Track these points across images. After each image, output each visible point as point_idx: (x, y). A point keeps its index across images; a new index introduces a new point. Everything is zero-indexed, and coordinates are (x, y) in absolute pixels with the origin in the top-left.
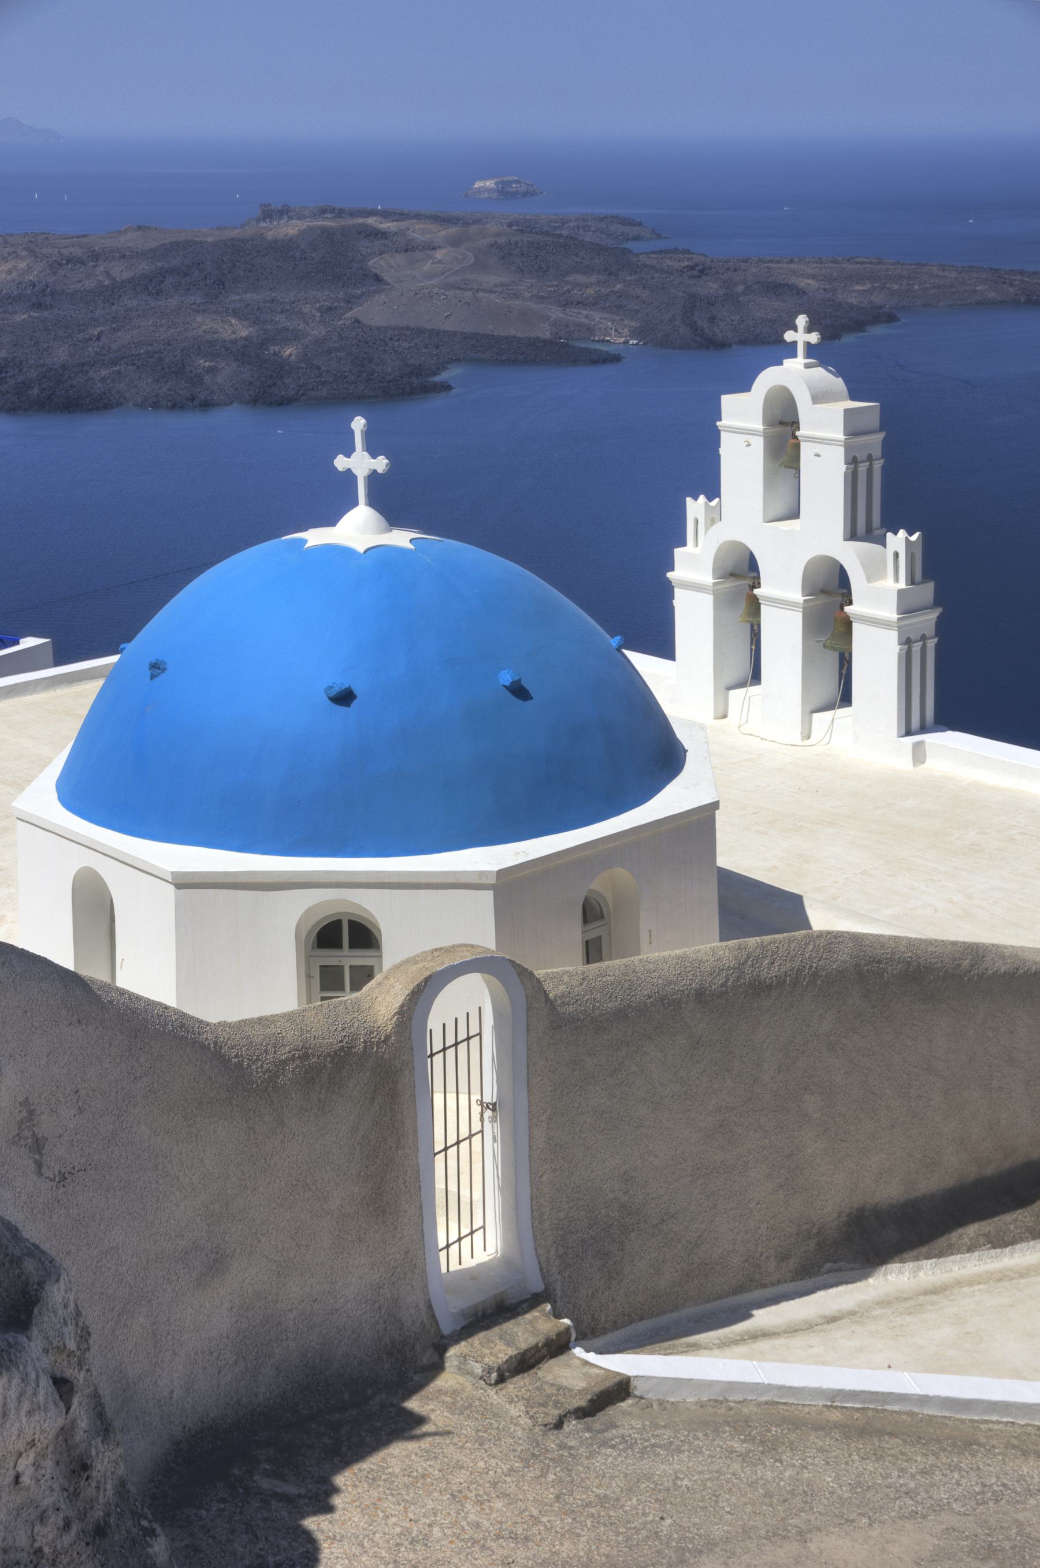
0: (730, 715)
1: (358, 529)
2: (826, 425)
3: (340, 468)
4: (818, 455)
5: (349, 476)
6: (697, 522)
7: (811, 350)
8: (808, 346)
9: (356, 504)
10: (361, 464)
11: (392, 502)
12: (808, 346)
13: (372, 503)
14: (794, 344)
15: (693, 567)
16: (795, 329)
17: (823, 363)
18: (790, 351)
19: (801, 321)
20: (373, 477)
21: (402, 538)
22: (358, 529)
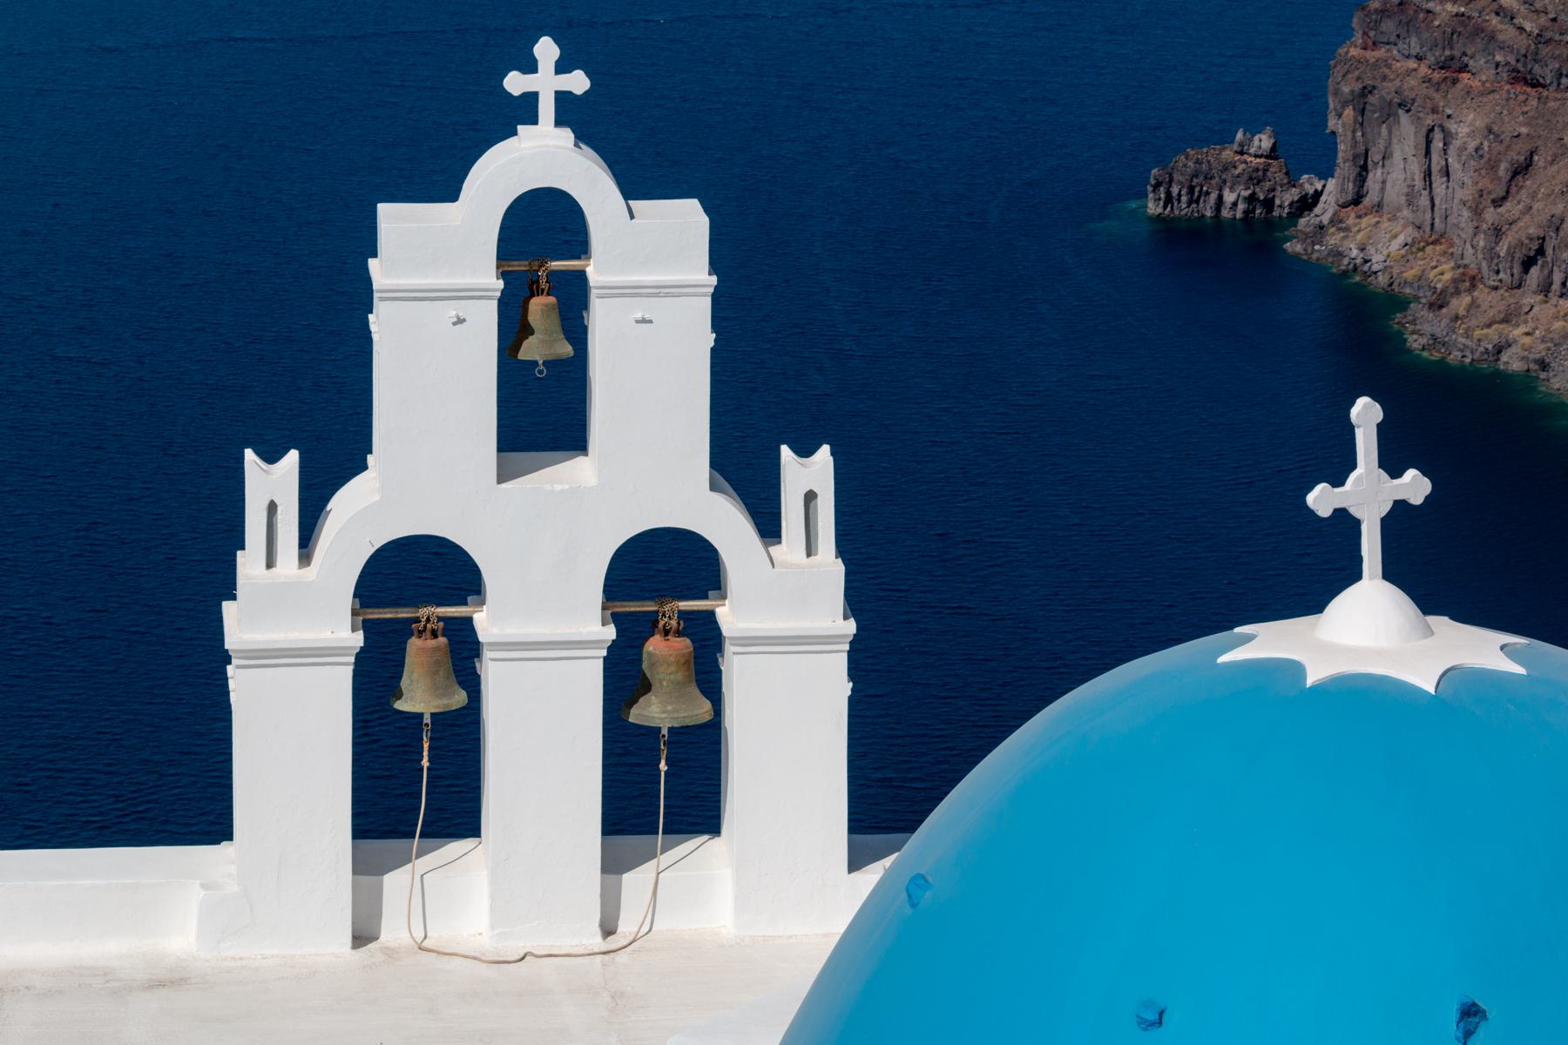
0: (1454, 1016)
1: (1368, 631)
2: (654, 270)
3: (1324, 512)
4: (460, 321)
5: (1345, 523)
6: (272, 508)
7: (569, 110)
8: (562, 98)
9: (1357, 576)
10: (1368, 492)
11: (1435, 568)
12: (562, 98)
13: (1390, 574)
14: (531, 99)
15: (287, 623)
16: (562, 67)
17: (583, 137)
18: (526, 109)
19: (546, 50)
20: (1399, 518)
21: (1485, 650)
22: (1368, 631)
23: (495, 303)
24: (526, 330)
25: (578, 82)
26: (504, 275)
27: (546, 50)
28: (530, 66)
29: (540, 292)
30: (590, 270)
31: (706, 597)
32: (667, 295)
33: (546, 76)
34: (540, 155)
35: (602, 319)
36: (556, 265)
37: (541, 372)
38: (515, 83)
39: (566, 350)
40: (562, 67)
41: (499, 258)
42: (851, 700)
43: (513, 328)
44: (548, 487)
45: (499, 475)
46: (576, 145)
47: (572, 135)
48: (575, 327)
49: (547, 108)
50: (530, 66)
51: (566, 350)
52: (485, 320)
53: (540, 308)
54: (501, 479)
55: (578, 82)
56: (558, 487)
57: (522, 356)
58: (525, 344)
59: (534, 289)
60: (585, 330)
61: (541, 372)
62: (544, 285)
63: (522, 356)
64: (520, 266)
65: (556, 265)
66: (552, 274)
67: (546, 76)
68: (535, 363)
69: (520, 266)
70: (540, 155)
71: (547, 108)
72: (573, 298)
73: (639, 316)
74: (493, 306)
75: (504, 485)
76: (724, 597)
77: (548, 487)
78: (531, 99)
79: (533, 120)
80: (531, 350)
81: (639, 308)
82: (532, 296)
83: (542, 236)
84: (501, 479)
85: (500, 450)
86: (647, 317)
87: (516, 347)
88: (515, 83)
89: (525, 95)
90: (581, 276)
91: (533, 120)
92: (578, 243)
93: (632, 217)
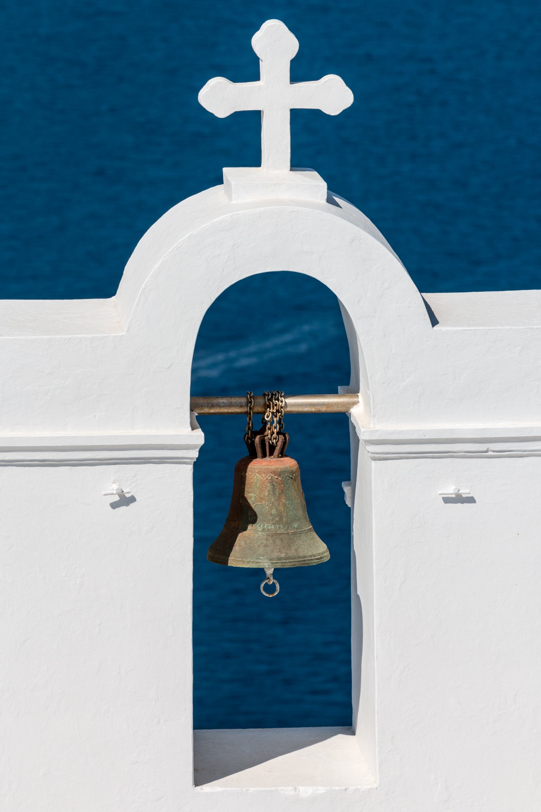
4: (125, 500)
7: (315, 142)
8: (304, 122)
12: (304, 122)
14: (249, 122)
16: (303, 70)
18: (240, 140)
19: (274, 42)
23: (188, 470)
24: (242, 515)
25: (332, 95)
26: (202, 421)
27: (274, 42)
28: (246, 69)
29: (268, 450)
30: (359, 414)
31: (334, 392)
32: (501, 455)
33: (275, 84)
34: (267, 217)
35: (384, 501)
36: (295, 403)
37: (270, 589)
38: (219, 97)
39: (317, 550)
40: (303, 70)
41: (194, 394)
42: (318, 112)
43: (221, 512)
44: (288, 791)
45: (196, 770)
46: (330, 201)
47: (324, 185)
48: (328, 505)
49: (276, 138)
50: (246, 69)
51: (317, 550)
52: (171, 501)
53: (265, 477)
54: (203, 773)
55: (332, 95)
56: (306, 791)
57: (239, 558)
58: (242, 539)
59: (254, 447)
60: (347, 514)
61: (271, 589)
62: (272, 434)
63: (236, 560)
64: (231, 406)
65: (295, 403)
66: (293, 421)
67: (275, 84)
68: (260, 573)
69: (231, 406)
70: (267, 217)
71: (276, 138)
72: (327, 461)
73: (450, 490)
74: (185, 475)
75: (206, 788)
76: (356, 391)
77: (288, 791)
78: (249, 122)
79: (252, 157)
80: (254, 550)
81: (451, 477)
82: (253, 455)
83: (272, 356)
84: (203, 773)
85: (201, 721)
86: (465, 492)
87: (225, 544)
88: (219, 97)
89: (238, 116)
90: (341, 422)
91: (252, 157)
92: (336, 367)
93: (434, 322)
